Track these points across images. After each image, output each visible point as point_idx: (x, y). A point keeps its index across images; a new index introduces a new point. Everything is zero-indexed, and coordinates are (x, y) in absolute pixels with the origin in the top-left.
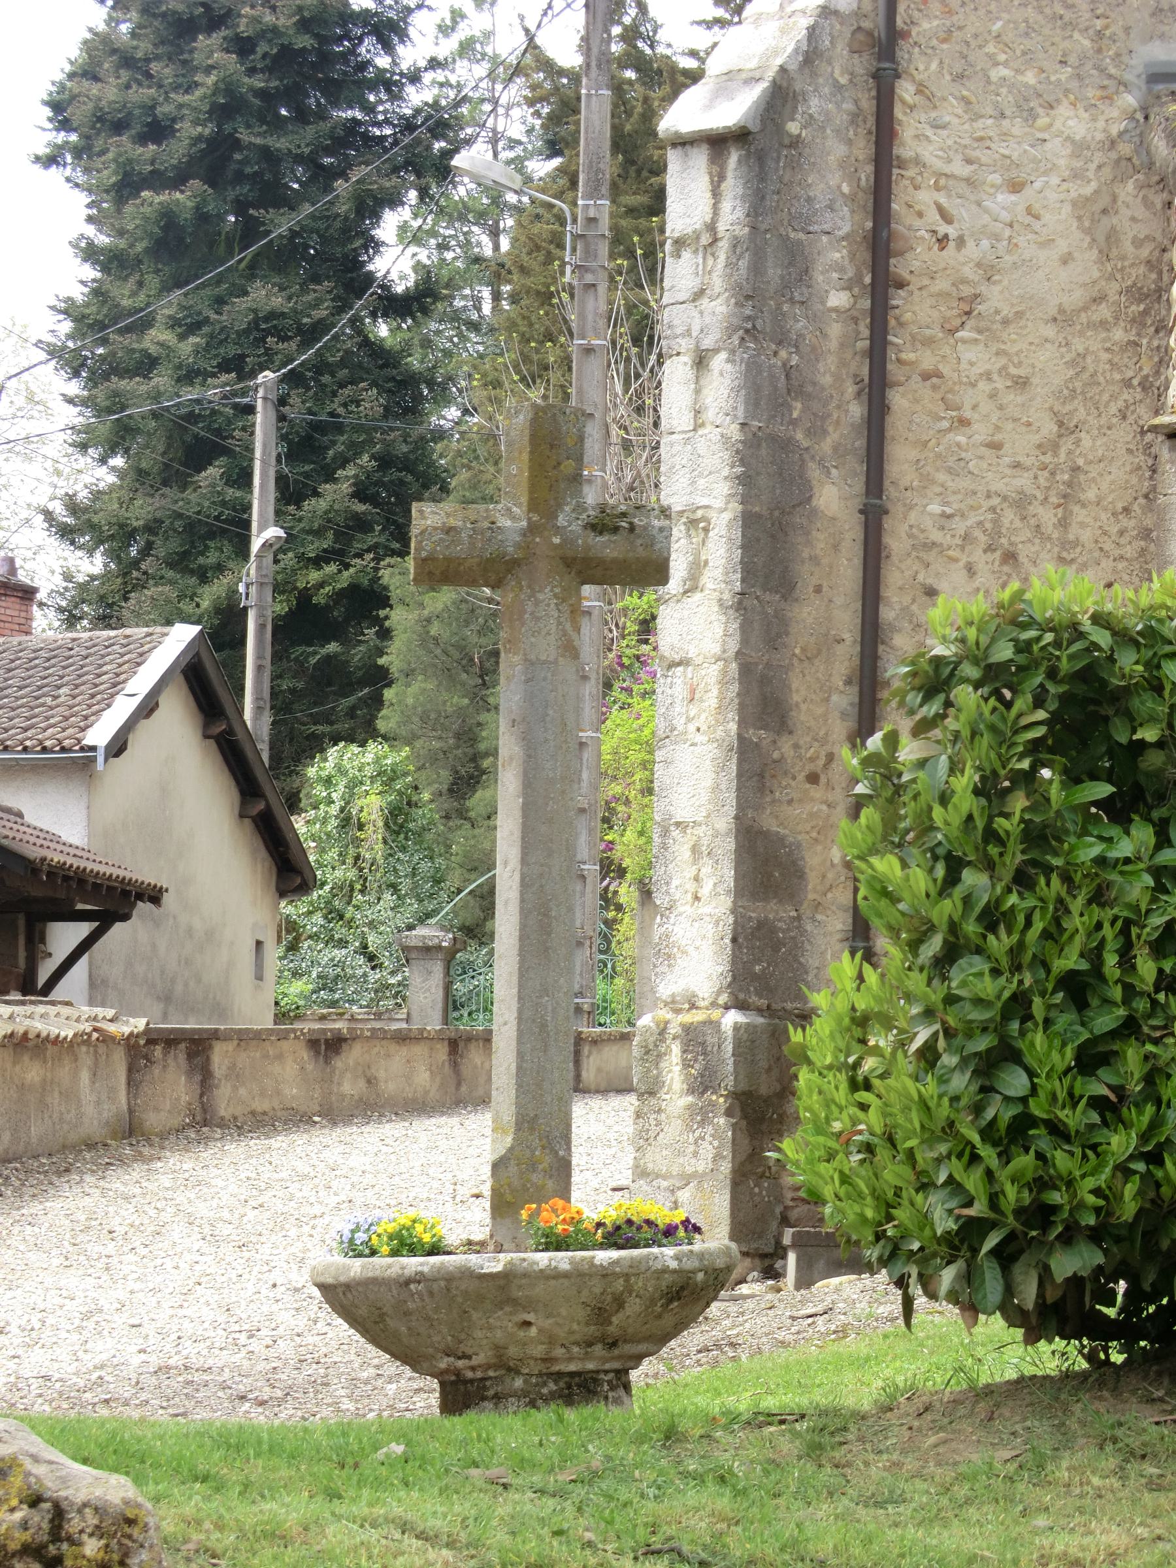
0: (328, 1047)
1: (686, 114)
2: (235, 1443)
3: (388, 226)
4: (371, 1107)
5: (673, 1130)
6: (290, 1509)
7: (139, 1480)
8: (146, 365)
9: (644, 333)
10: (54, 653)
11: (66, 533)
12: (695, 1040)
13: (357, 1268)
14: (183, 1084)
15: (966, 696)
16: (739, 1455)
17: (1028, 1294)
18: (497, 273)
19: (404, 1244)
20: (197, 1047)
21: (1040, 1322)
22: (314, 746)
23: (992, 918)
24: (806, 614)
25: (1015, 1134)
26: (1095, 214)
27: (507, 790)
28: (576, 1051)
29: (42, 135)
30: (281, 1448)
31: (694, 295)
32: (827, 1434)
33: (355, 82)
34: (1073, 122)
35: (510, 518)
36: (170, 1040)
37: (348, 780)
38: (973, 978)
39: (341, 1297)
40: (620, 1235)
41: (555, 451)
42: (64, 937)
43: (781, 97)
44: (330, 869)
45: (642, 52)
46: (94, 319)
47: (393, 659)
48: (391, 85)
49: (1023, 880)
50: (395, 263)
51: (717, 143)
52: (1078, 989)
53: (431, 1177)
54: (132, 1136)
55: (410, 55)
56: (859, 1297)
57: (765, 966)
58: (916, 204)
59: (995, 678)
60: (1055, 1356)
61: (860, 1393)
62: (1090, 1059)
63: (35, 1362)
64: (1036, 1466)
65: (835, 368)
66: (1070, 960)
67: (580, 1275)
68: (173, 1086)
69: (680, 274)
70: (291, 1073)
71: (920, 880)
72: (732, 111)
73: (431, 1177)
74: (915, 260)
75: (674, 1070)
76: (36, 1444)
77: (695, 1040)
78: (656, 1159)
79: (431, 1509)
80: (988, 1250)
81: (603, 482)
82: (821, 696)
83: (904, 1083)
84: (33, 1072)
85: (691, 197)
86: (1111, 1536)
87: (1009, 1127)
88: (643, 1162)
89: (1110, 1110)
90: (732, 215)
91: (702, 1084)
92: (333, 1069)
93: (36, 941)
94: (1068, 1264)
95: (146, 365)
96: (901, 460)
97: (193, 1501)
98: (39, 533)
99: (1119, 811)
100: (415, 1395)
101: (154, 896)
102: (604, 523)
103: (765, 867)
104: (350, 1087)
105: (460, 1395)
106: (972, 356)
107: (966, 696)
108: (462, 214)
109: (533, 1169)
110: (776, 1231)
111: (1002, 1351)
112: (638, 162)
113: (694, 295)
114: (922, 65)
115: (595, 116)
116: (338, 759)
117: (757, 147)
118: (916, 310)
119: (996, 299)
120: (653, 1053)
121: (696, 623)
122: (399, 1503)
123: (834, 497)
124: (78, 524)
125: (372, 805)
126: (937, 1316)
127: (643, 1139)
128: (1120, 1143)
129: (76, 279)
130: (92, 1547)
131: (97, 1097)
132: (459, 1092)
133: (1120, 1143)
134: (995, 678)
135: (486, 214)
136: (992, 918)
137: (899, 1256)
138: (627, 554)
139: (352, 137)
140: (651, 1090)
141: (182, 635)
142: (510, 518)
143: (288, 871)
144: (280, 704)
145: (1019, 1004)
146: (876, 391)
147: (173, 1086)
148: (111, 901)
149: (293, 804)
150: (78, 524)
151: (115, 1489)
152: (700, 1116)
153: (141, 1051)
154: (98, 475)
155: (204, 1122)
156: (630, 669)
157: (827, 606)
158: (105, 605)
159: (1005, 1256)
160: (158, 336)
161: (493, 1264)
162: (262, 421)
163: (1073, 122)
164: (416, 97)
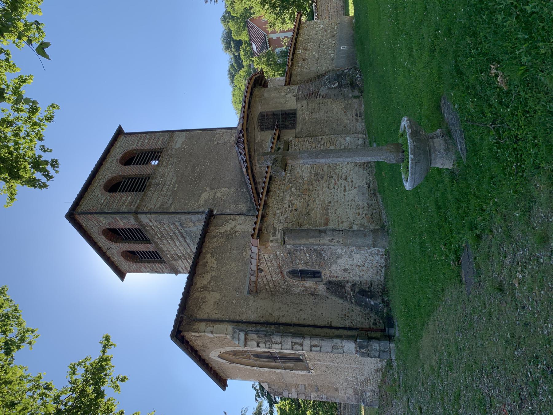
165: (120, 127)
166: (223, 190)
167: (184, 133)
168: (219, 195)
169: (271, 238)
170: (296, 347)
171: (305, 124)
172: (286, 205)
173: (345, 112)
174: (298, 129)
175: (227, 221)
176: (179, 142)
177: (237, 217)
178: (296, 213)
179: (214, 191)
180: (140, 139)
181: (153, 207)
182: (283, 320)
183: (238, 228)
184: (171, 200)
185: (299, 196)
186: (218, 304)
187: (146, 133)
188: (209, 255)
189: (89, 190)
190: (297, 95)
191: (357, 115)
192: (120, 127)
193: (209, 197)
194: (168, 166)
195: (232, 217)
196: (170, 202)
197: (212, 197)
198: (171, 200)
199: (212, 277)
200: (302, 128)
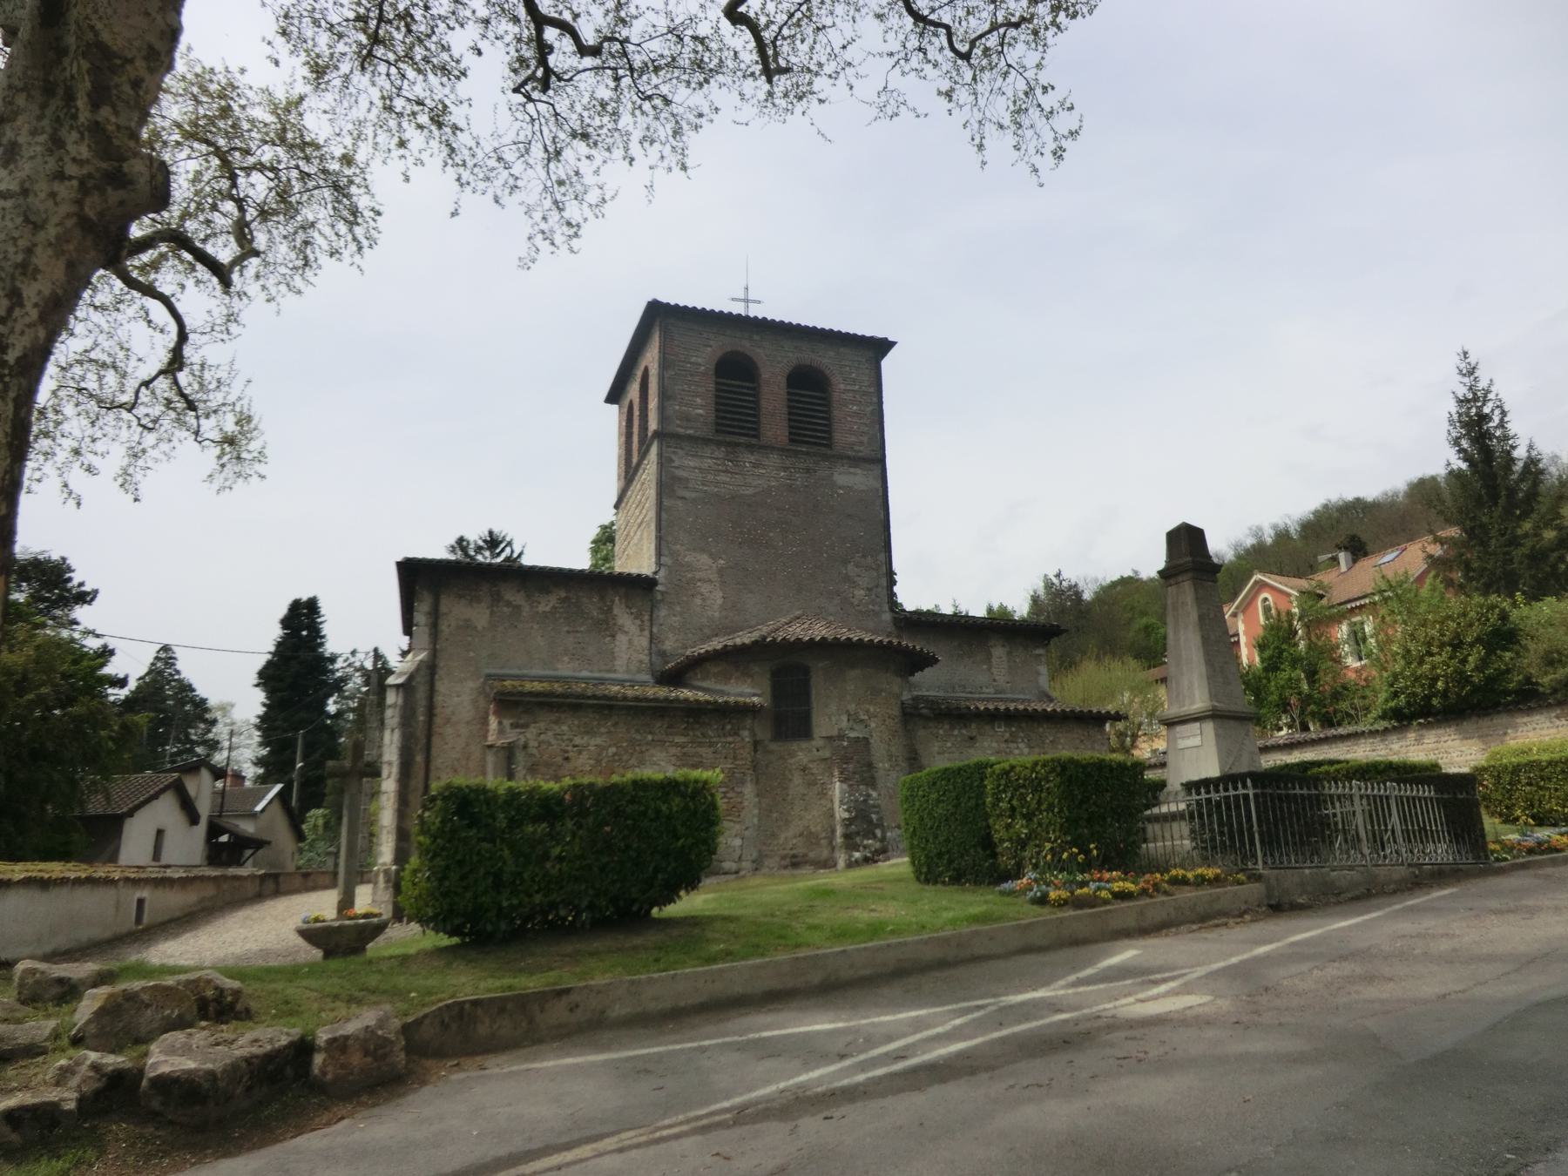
0: (306, 875)
1: (391, 680)
2: (269, 970)
3: (331, 701)
4: (314, 888)
5: (380, 892)
6: (279, 986)
7: (243, 982)
8: (276, 729)
9: (382, 723)
10: (250, 790)
11: (256, 764)
12: (386, 872)
13: (305, 926)
14: (274, 885)
15: (439, 802)
16: (384, 967)
17: (449, 927)
18: (353, 710)
19: (317, 920)
20: (276, 877)
21: (451, 934)
22: (309, 810)
23: (443, 849)
24: (413, 783)
25: (445, 895)
26: (474, 702)
27: (345, 820)
28: (360, 873)
29: (254, 679)
30: (279, 971)
31: (392, 716)
32: (404, 960)
33: (326, 671)
34: (471, 684)
35: (347, 764)
36: (270, 875)
37: (316, 816)
38: (439, 861)
39: (303, 933)
40: (366, 916)
41: (358, 749)
42: (248, 852)
43: (411, 677)
44: (310, 837)
45: (686, 700)
46: (264, 719)
47: (327, 791)
48: (333, 671)
49: (449, 841)
50: (332, 708)
51: (397, 686)
52: (460, 863)
53: (322, 905)
54: (259, 897)
55: (337, 666)
56: (415, 927)
57: (401, 856)
58: (439, 699)
59: (445, 799)
60: (455, 940)
61: (412, 951)
62: (463, 878)
63: (232, 949)
64: (449, 965)
65: (420, 732)
66: (459, 857)
67: (357, 926)
68: (270, 885)
69: (389, 713)
70: (298, 881)
71: (428, 841)
72: (400, 681)
73: (322, 905)
74: (438, 711)
75: (381, 878)
76: (218, 975)
77: (386, 872)
78: (377, 898)
79: (314, 983)
80: (438, 920)
81: (369, 755)
82: (416, 799)
83: (423, 884)
84: (237, 884)
85: (391, 698)
86: (463, 979)
87: (159, 1076)
88: (366, 899)
89: (466, 888)
90: (400, 701)
91: (387, 881)
92: (308, 881)
93: (241, 854)
94: (457, 921)
95: (276, 729)
96: (434, 751)
97: (257, 985)
98: (249, 764)
99: (470, 826)
100: (317, 954)
101: (269, 843)
102: (369, 765)
103: (402, 835)
104: (311, 884)
105: (328, 954)
106: (449, 730)
107: (439, 802)
108: (347, 698)
109: (346, 902)
110: (398, 915)
111: (445, 941)
112: (382, 689)
113: (392, 716)
114: (441, 672)
115: (374, 680)
116: (313, 812)
117: (406, 688)
118: (438, 720)
119: (454, 719)
120: (377, 874)
121: (389, 785)
122: (305, 983)
123: (419, 758)
124: (259, 762)
125: (321, 822)
126: (430, 932)
127: (374, 893)
128: (469, 895)
129: (261, 710)
130: (229, 999)
131: (251, 888)
132: (333, 885)
133: (469, 895)
134: (445, 799)
135: (351, 698)
136: (443, 849)
137: (423, 921)
138: (374, 772)
139: (324, 682)
140: (376, 883)
141: (278, 787)
142: (347, 764)
143: (300, 836)
144: (300, 799)
145: (447, 867)
146: (429, 736)
147: (270, 885)
148: (257, 844)
149: (303, 822)
150: (259, 762)
151: (236, 984)
152: (386, 888)
153: (263, 878)
154: (264, 752)
155: (278, 893)
156: (375, 794)
157: (417, 782)
158: (264, 780)
159: (444, 920)
160: (278, 723)
161: (337, 924)
162: (300, 742)
163: (471, 684)
164: (338, 674)
165: (893, 344)
166: (718, 595)
167: (878, 485)
168: (705, 589)
169: (507, 722)
170: (1364, 801)
171: (782, 758)
172: (577, 741)
173: (801, 835)
174: (773, 746)
175: (638, 616)
176: (849, 479)
177: (647, 633)
178: (559, 759)
179: (714, 577)
180: (865, 393)
181: (676, 464)
182: (436, 740)
183: (621, 638)
184: (694, 495)
185: (598, 761)
186: (468, 625)
187: (880, 403)
188: (563, 594)
189: (108, 934)
190: (841, 737)
191: (794, 856)
192: (893, 344)
193: (700, 570)
194: (785, 469)
195: (647, 624)
196: (687, 494)
197: (699, 575)
198: (694, 495)
199: (518, 607)
200: (771, 752)
